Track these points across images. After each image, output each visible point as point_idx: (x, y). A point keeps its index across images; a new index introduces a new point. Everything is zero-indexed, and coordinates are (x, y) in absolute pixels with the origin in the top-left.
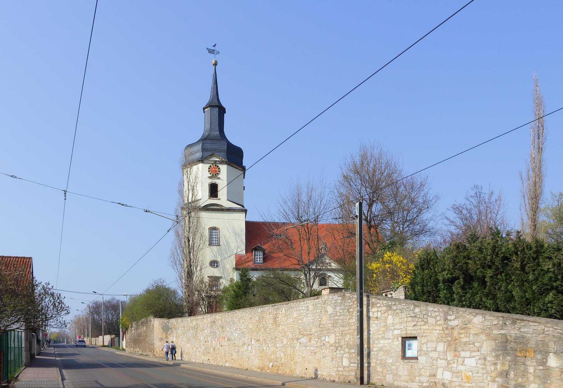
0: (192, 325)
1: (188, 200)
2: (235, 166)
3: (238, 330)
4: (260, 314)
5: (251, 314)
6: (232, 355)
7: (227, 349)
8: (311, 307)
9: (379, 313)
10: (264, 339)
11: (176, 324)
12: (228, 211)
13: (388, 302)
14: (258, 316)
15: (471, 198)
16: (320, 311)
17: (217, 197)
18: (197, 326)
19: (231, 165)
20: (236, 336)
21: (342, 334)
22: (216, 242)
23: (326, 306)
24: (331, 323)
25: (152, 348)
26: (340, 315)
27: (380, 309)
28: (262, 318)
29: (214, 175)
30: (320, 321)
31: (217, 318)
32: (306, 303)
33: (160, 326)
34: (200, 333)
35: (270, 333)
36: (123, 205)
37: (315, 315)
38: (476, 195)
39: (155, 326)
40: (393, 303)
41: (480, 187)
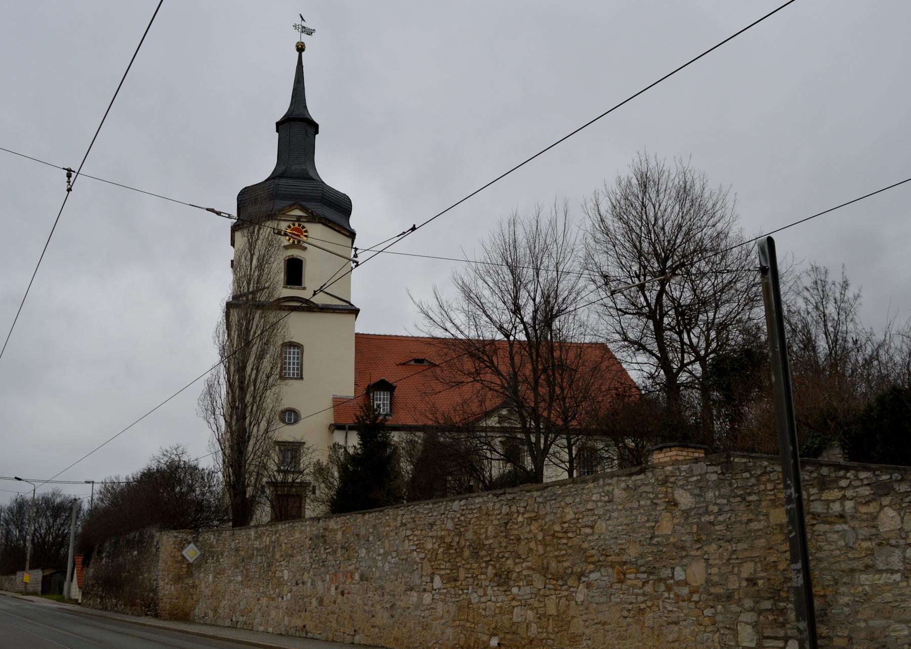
0: (260, 544)
1: (248, 289)
2: (336, 228)
3: (391, 555)
4: (458, 515)
5: (430, 514)
6: (373, 616)
7: (359, 602)
8: (619, 493)
9: (849, 505)
10: (470, 575)
11: (215, 543)
12: (320, 312)
13: (878, 473)
14: (453, 519)
15: (805, 290)
16: (649, 502)
17: (301, 285)
18: (274, 548)
19: (330, 225)
20: (387, 568)
21: (729, 560)
22: (296, 372)
23: (670, 490)
24: (688, 533)
25: (152, 598)
26: (720, 512)
27: (849, 493)
28: (464, 524)
29: (296, 243)
30: (653, 527)
31: (330, 527)
32: (604, 485)
33: (175, 548)
34: (282, 563)
35: (491, 560)
36: (219, 213)
37: (635, 512)
38: (815, 286)
39: (162, 549)
40: (897, 476)
41: (823, 271)
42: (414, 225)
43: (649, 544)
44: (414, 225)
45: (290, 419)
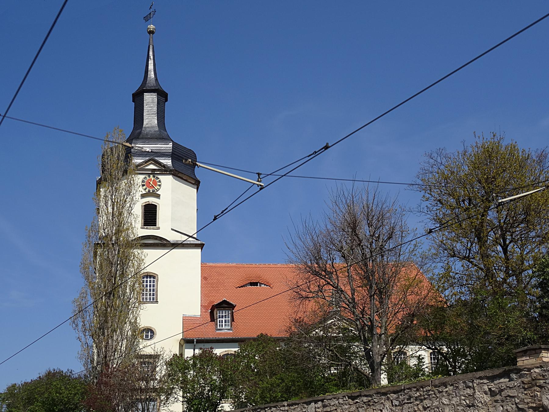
19: (178, 175)
42: (327, 144)
43: (315, 408)
44: (327, 144)
45: (147, 336)
